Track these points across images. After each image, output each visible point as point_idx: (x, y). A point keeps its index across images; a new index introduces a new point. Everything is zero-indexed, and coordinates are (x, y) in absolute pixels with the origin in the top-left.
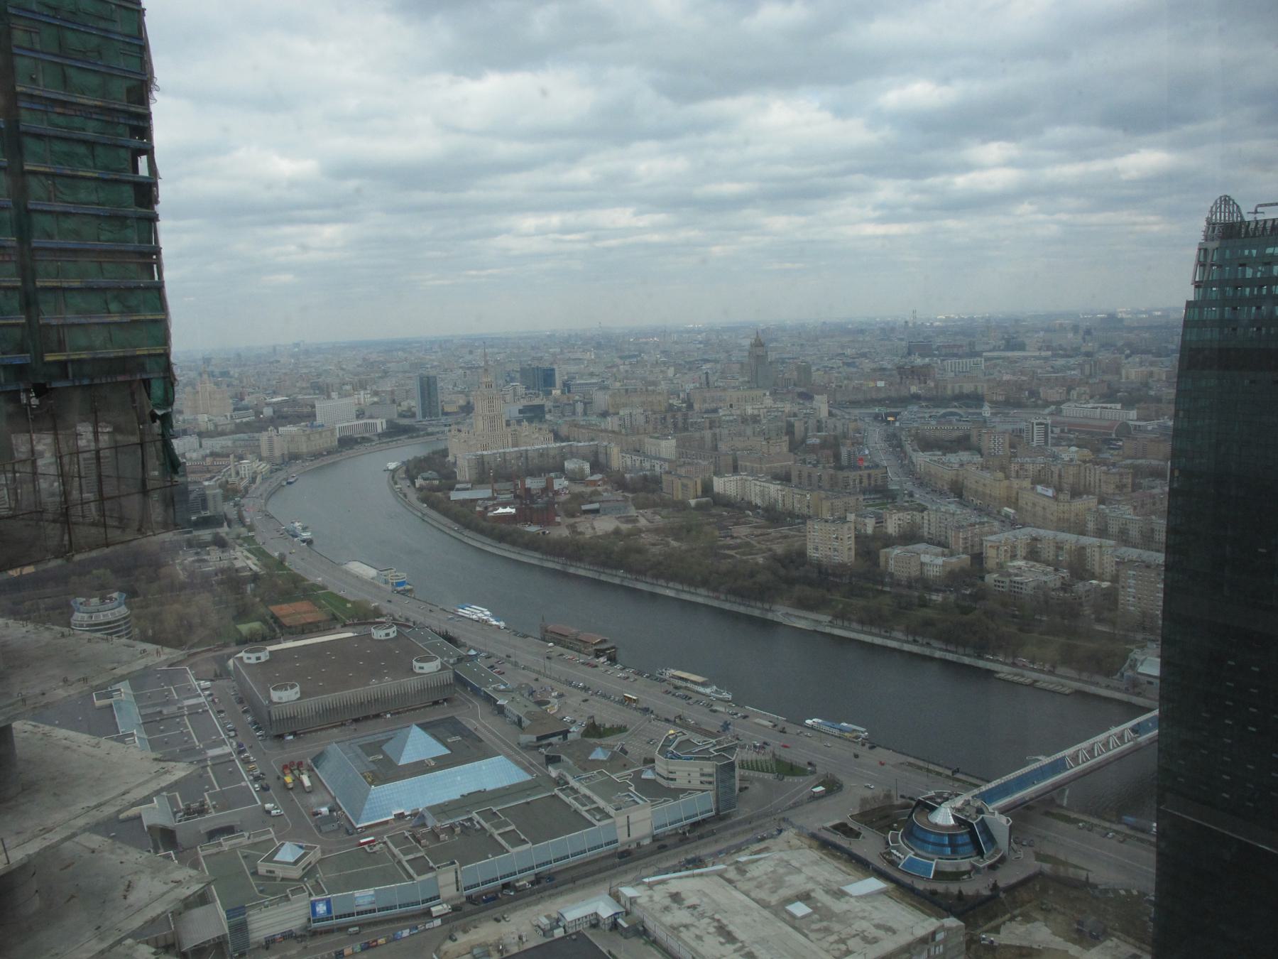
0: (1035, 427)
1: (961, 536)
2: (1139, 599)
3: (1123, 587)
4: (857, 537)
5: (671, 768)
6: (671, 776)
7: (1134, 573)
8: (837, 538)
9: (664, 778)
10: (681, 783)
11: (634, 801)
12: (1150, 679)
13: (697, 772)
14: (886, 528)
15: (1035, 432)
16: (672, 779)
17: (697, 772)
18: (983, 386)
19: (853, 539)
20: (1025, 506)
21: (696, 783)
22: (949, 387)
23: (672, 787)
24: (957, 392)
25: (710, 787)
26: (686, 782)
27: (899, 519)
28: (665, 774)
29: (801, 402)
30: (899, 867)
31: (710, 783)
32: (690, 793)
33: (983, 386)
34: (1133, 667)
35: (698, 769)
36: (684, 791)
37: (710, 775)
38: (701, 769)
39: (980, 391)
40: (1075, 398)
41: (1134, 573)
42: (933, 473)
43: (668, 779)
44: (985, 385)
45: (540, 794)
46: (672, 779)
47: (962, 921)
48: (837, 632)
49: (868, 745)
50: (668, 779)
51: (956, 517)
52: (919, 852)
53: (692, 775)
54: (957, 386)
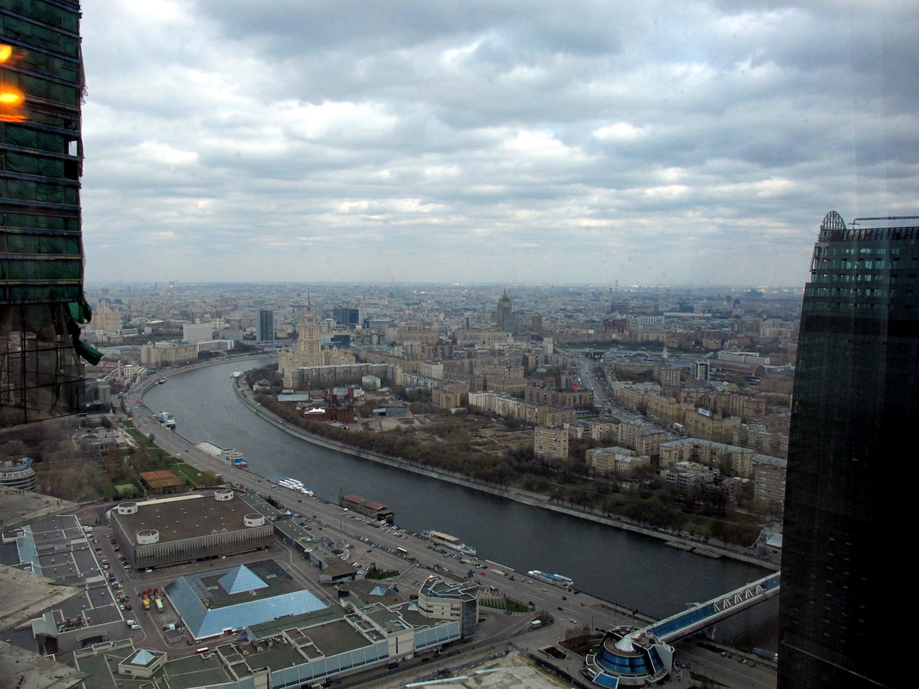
0: (699, 366)
3: (757, 483)
6: (429, 609)
8: (556, 440)
9: (424, 610)
10: (436, 615)
11: (402, 626)
14: (591, 435)
16: (430, 612)
18: (663, 337)
21: (447, 615)
22: (639, 336)
24: (645, 339)
28: (425, 607)
30: (593, 681)
31: (458, 615)
32: (442, 623)
33: (663, 337)
35: (449, 605)
36: (438, 620)
38: (452, 605)
39: (661, 339)
46: (430, 612)
47: (456, 537)
49: (573, 591)
50: (427, 611)
53: (445, 608)
54: (645, 335)
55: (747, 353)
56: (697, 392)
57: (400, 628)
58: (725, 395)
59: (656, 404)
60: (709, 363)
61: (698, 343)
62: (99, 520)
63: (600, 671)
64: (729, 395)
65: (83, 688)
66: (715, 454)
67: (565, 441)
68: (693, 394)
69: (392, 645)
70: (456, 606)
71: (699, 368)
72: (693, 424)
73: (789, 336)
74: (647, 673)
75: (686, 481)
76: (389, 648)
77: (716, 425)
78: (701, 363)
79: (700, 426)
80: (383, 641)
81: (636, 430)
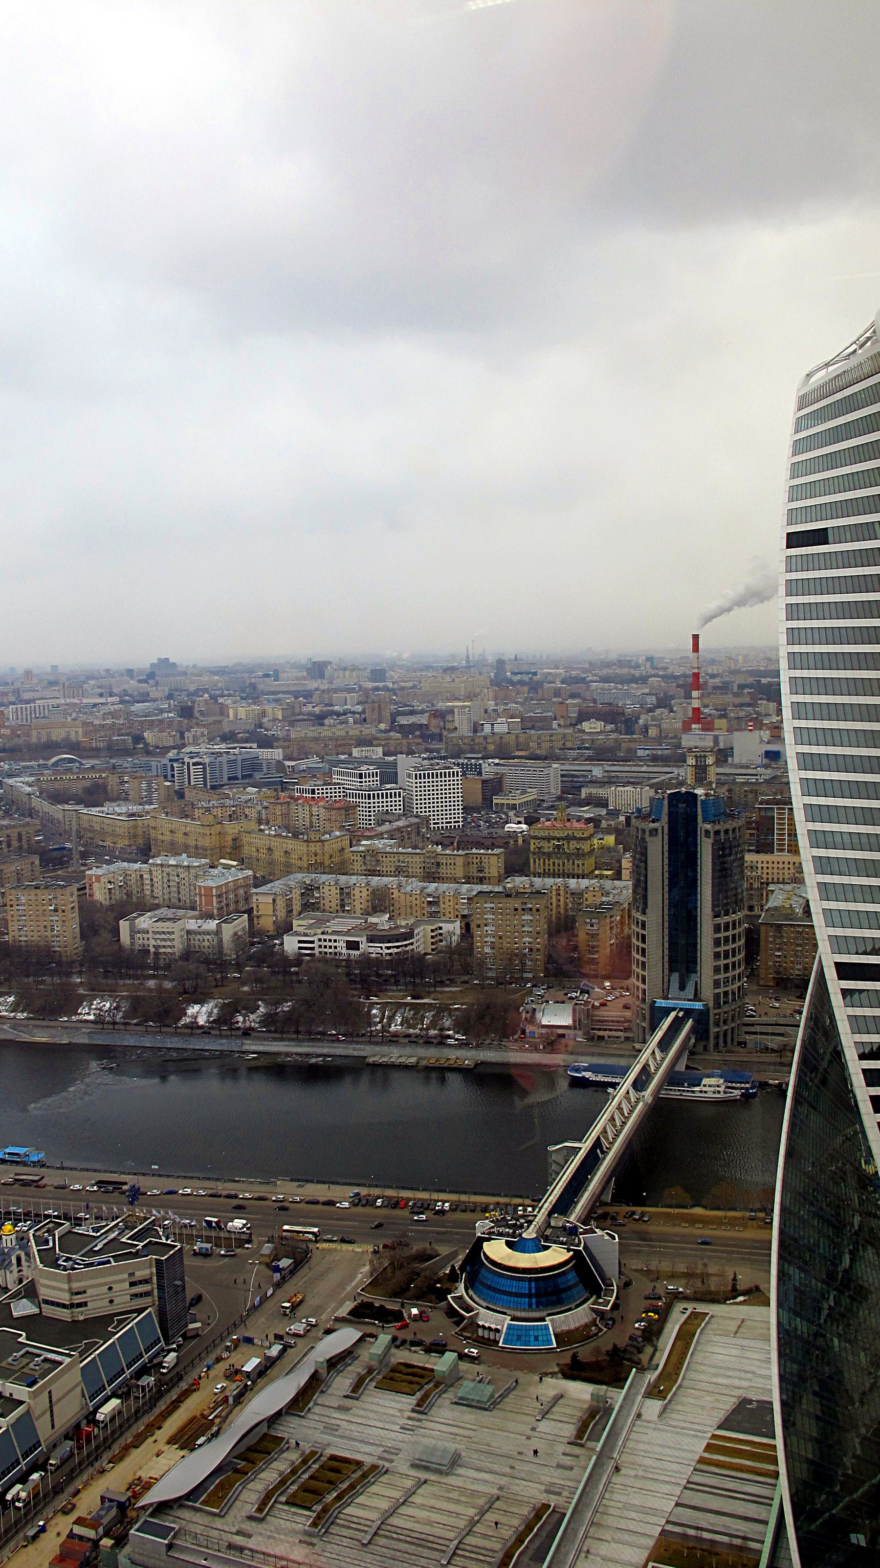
0: (192, 767)
1: (214, 893)
2: (500, 938)
3: (479, 926)
4: (81, 908)
5: (76, 1286)
6: (78, 1299)
7: (492, 905)
8: (56, 910)
9: (64, 1306)
10: (97, 1307)
11: (46, 1360)
12: (560, 1031)
13: (123, 1281)
14: (91, 895)
15: (192, 774)
16: (79, 1305)
17: (123, 1281)
18: (77, 732)
19: (77, 909)
20: (255, 854)
21: (123, 1301)
22: (34, 733)
23: (81, 1318)
24: (44, 739)
25: (148, 1300)
26: (106, 1302)
27: (110, 882)
28: (65, 1298)
29: (137, 707)
30: (500, 1344)
31: (147, 1294)
32: (120, 1322)
33: (77, 732)
34: (532, 1020)
35: (126, 1276)
36: (107, 1319)
37: (147, 1281)
38: (132, 1274)
39: (73, 737)
40: (191, 741)
41: (492, 905)
42: (97, 827)
43: (72, 1306)
44: (80, 730)
45: (723, 1455)
46: (79, 1305)
48: (41, 1037)
50: (72, 1306)
51: (192, 871)
52: (519, 1314)
53: (116, 1287)
54: (44, 733)
55: (243, 745)
56: (223, 806)
57: (47, 1366)
58: (281, 804)
59: (171, 831)
60: (207, 761)
61: (138, 739)
62: (70, 1434)
63: (505, 1319)
64: (288, 803)
65: (794, 1566)
66: (305, 904)
67: (73, 908)
68: (215, 810)
69: (43, 1414)
70: (140, 1274)
71: (192, 771)
72: (262, 856)
73: (280, 718)
74: (587, 1295)
75: (336, 947)
76: (36, 1424)
77: (313, 849)
78: (195, 760)
79: (278, 855)
80: (21, 1410)
81: (182, 876)
